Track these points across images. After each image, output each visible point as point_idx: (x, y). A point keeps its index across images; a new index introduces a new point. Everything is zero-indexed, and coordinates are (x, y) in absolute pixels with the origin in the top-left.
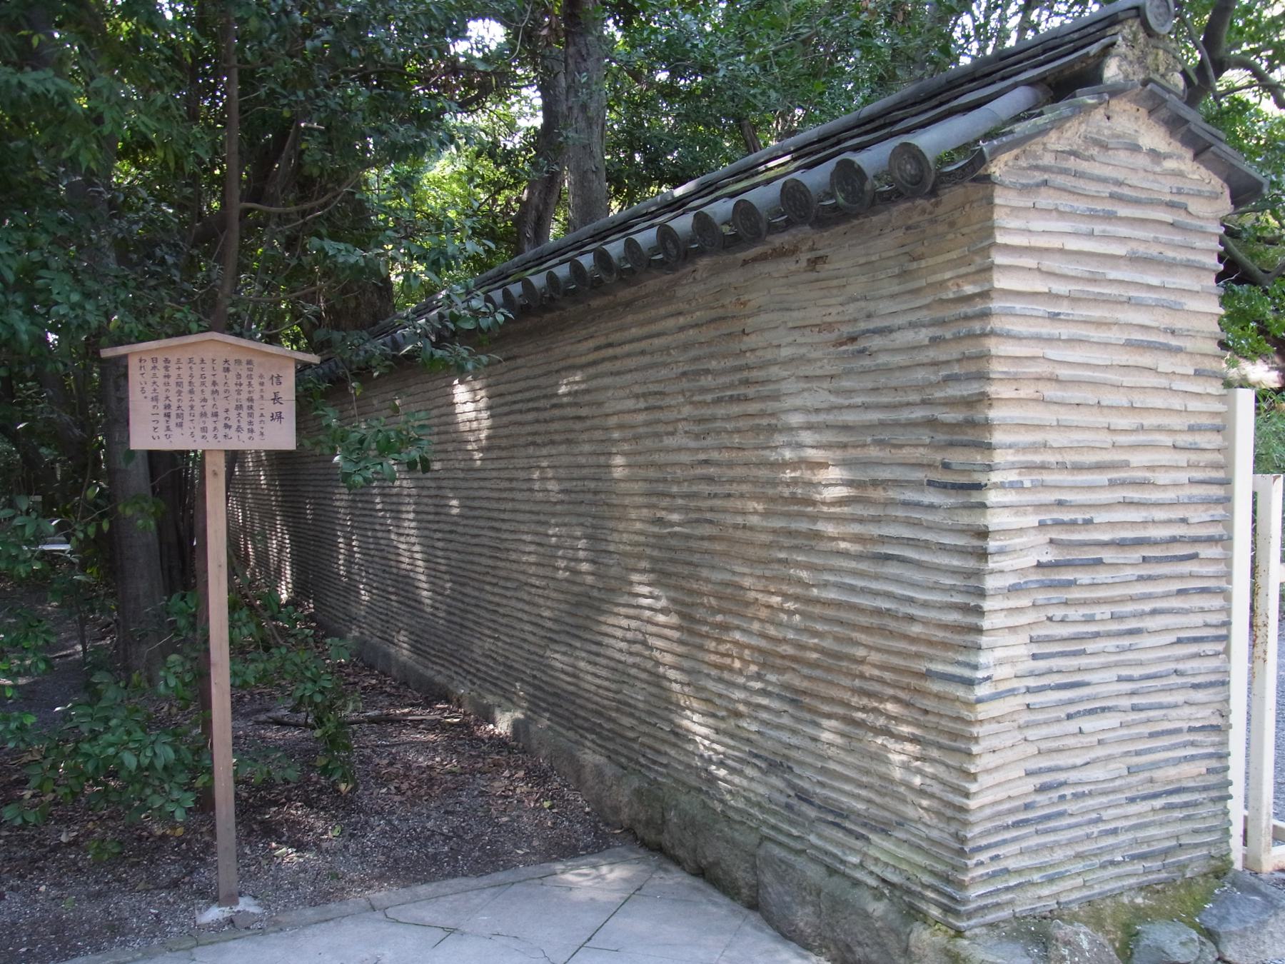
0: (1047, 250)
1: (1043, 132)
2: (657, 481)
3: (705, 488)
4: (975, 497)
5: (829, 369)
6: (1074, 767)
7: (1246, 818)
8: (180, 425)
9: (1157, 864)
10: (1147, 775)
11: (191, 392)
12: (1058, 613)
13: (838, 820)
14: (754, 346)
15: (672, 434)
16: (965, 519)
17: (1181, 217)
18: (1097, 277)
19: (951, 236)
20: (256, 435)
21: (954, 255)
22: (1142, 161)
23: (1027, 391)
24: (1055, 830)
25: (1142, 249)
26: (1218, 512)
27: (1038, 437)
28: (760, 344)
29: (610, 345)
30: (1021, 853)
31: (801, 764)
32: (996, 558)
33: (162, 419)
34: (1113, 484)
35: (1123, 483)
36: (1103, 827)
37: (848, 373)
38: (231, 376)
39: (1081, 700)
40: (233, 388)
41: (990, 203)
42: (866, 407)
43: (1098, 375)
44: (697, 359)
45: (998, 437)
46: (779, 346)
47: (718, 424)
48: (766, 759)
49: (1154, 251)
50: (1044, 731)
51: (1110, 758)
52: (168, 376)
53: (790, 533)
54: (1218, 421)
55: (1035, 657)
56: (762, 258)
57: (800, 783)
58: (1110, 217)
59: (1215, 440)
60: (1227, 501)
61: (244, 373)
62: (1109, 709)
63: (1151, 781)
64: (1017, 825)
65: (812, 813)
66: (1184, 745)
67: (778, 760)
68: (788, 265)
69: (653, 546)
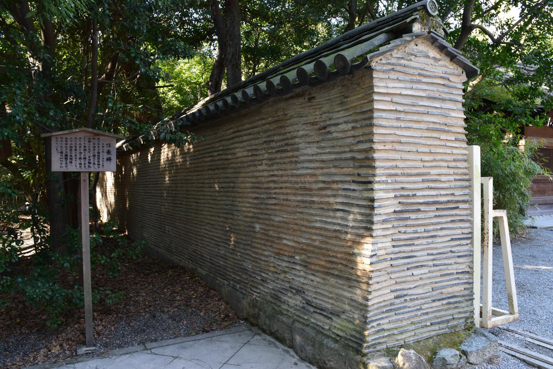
0: (395, 94)
1: (391, 50)
2: (256, 183)
3: (272, 185)
4: (370, 186)
5: (317, 139)
6: (410, 289)
7: (481, 307)
8: (71, 162)
9: (445, 325)
10: (440, 291)
11: (76, 150)
12: (403, 230)
13: (321, 312)
14: (290, 131)
15: (261, 165)
16: (366, 194)
17: (446, 82)
18: (415, 104)
19: (358, 89)
20: (101, 166)
21: (360, 96)
22: (432, 61)
23: (388, 147)
24: (403, 313)
25: (432, 94)
26: (467, 191)
27: (394, 164)
28: (292, 130)
29: (238, 131)
30: (389, 322)
31: (308, 290)
32: (377, 209)
33: (64, 160)
34: (423, 181)
35: (428, 181)
36: (422, 312)
37: (323, 140)
38: (91, 144)
39: (413, 263)
40: (92, 148)
41: (372, 78)
42: (330, 153)
43: (417, 141)
44: (269, 136)
45: (377, 164)
46: (298, 131)
47: (278, 161)
48: (295, 289)
49: (437, 95)
50: (398, 275)
51: (425, 285)
52: (67, 144)
53: (303, 202)
54: (465, 157)
55: (394, 246)
56: (292, 97)
57: (308, 298)
58: (419, 82)
59: (465, 165)
60: (470, 187)
61: (96, 143)
62: (424, 266)
63: (442, 293)
64: (387, 311)
65: (312, 309)
66: (455, 279)
67: (300, 289)
68: (301, 100)
69: (254, 208)
